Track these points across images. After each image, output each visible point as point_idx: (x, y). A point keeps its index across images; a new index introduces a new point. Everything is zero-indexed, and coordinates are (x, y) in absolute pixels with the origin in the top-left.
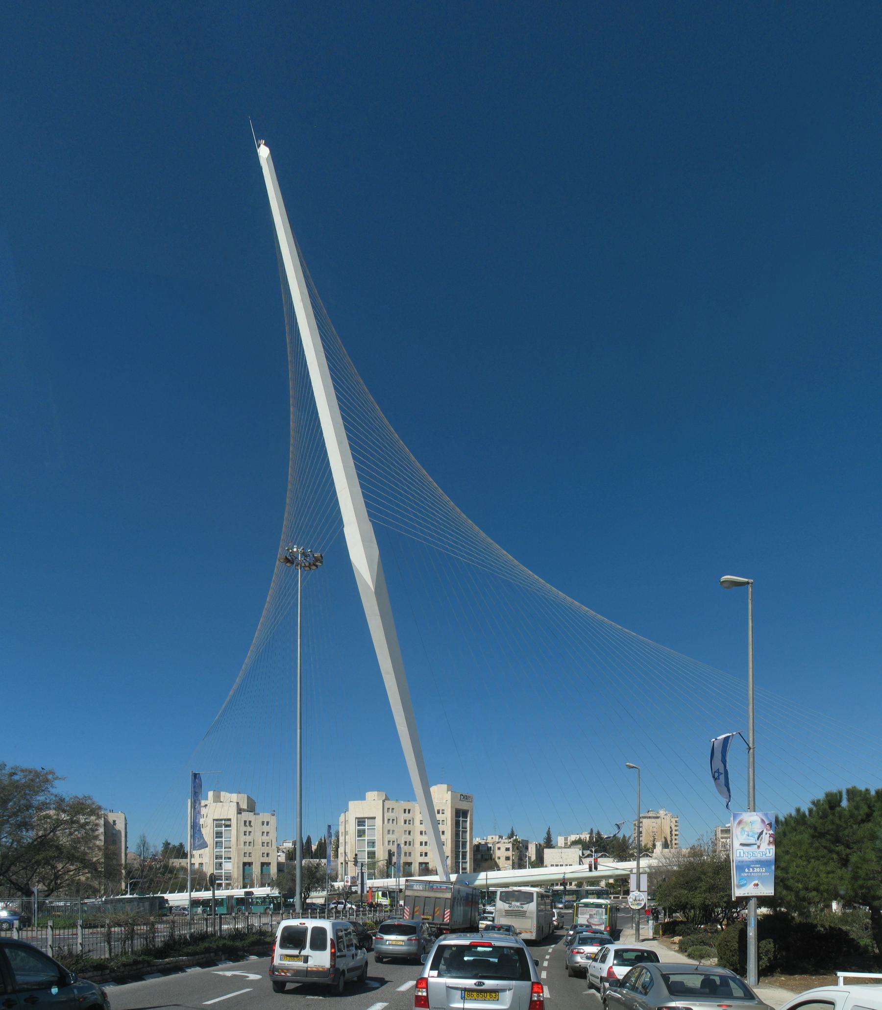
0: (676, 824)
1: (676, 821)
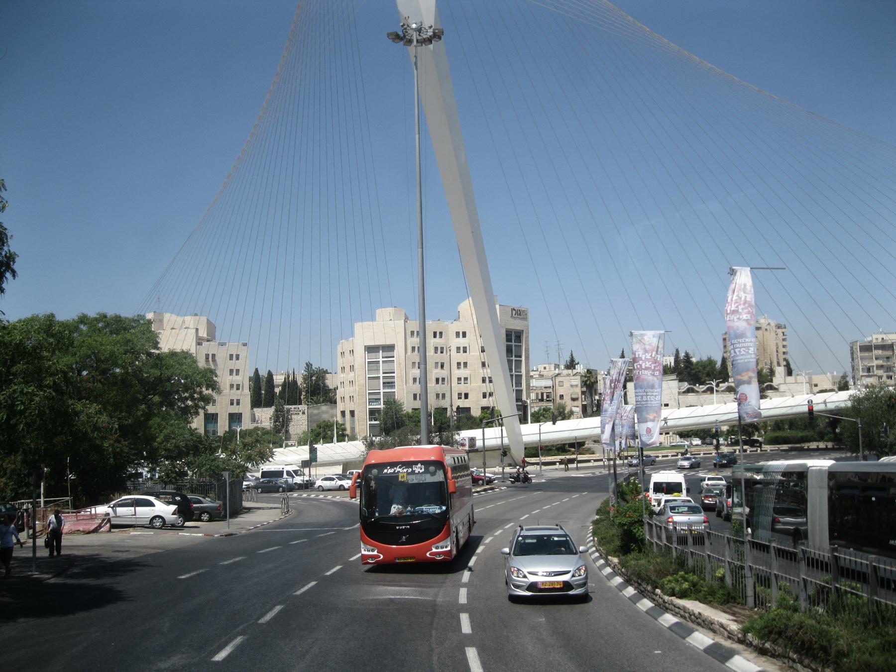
0: (784, 337)
1: (783, 333)
